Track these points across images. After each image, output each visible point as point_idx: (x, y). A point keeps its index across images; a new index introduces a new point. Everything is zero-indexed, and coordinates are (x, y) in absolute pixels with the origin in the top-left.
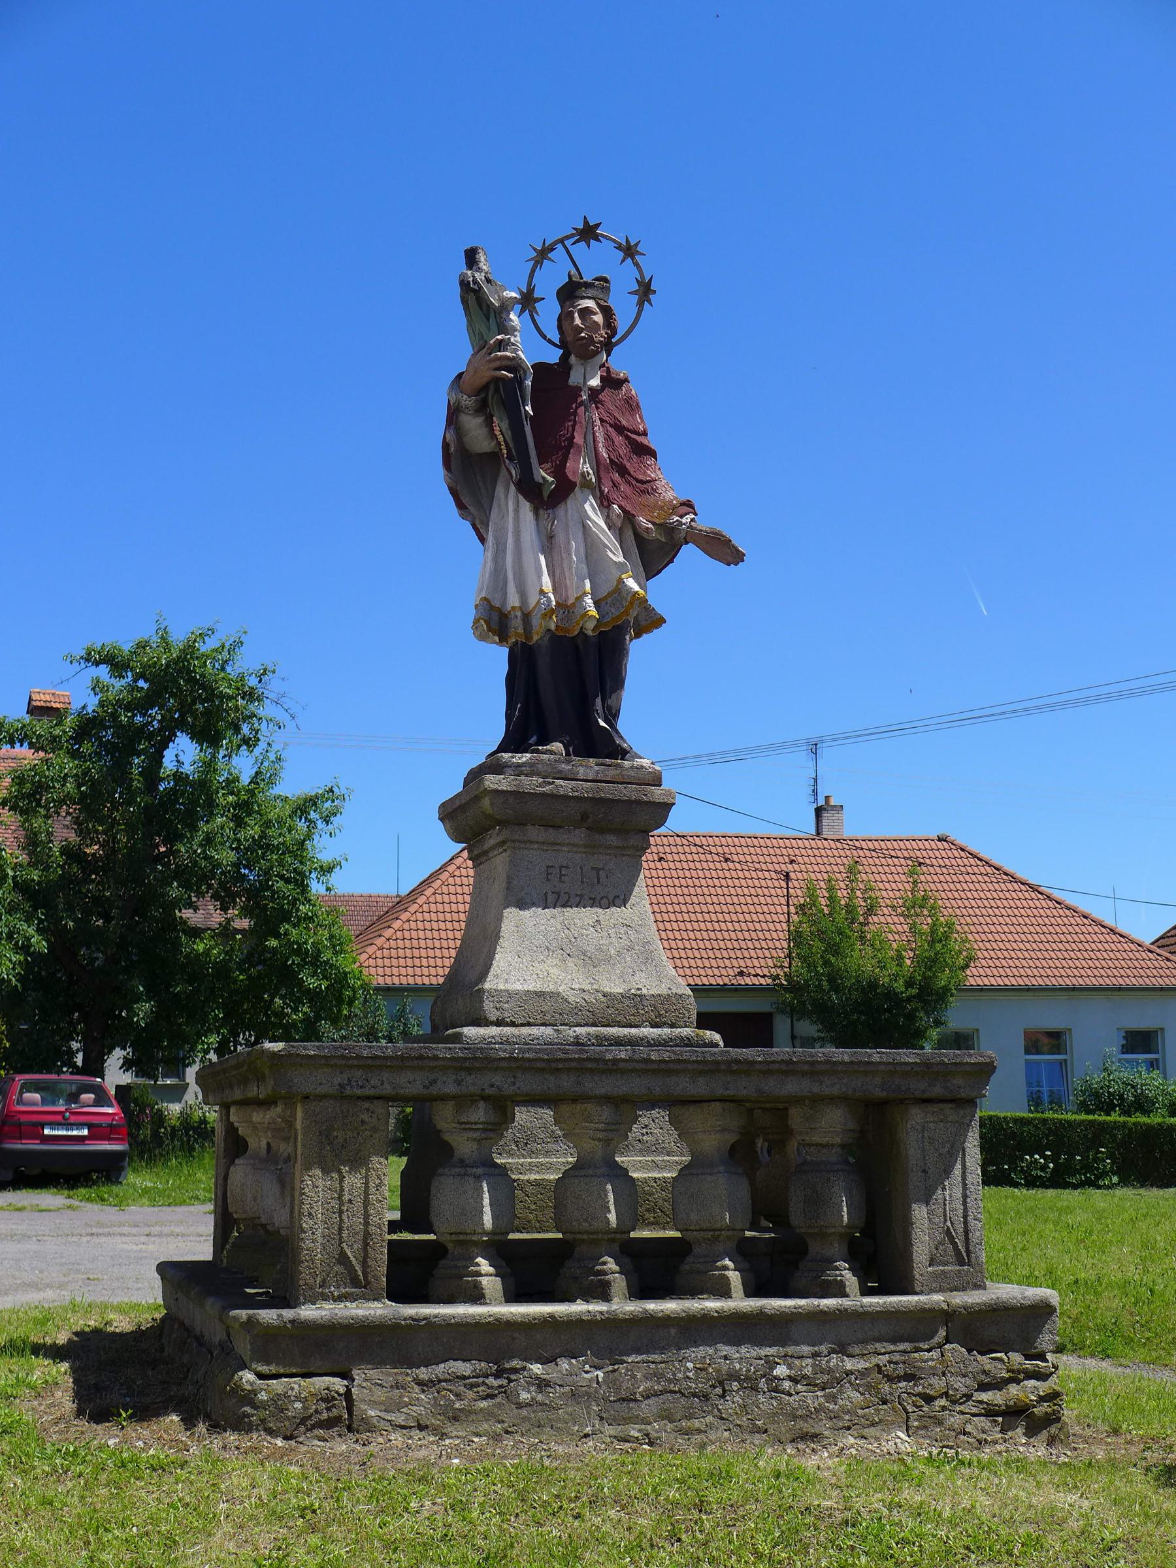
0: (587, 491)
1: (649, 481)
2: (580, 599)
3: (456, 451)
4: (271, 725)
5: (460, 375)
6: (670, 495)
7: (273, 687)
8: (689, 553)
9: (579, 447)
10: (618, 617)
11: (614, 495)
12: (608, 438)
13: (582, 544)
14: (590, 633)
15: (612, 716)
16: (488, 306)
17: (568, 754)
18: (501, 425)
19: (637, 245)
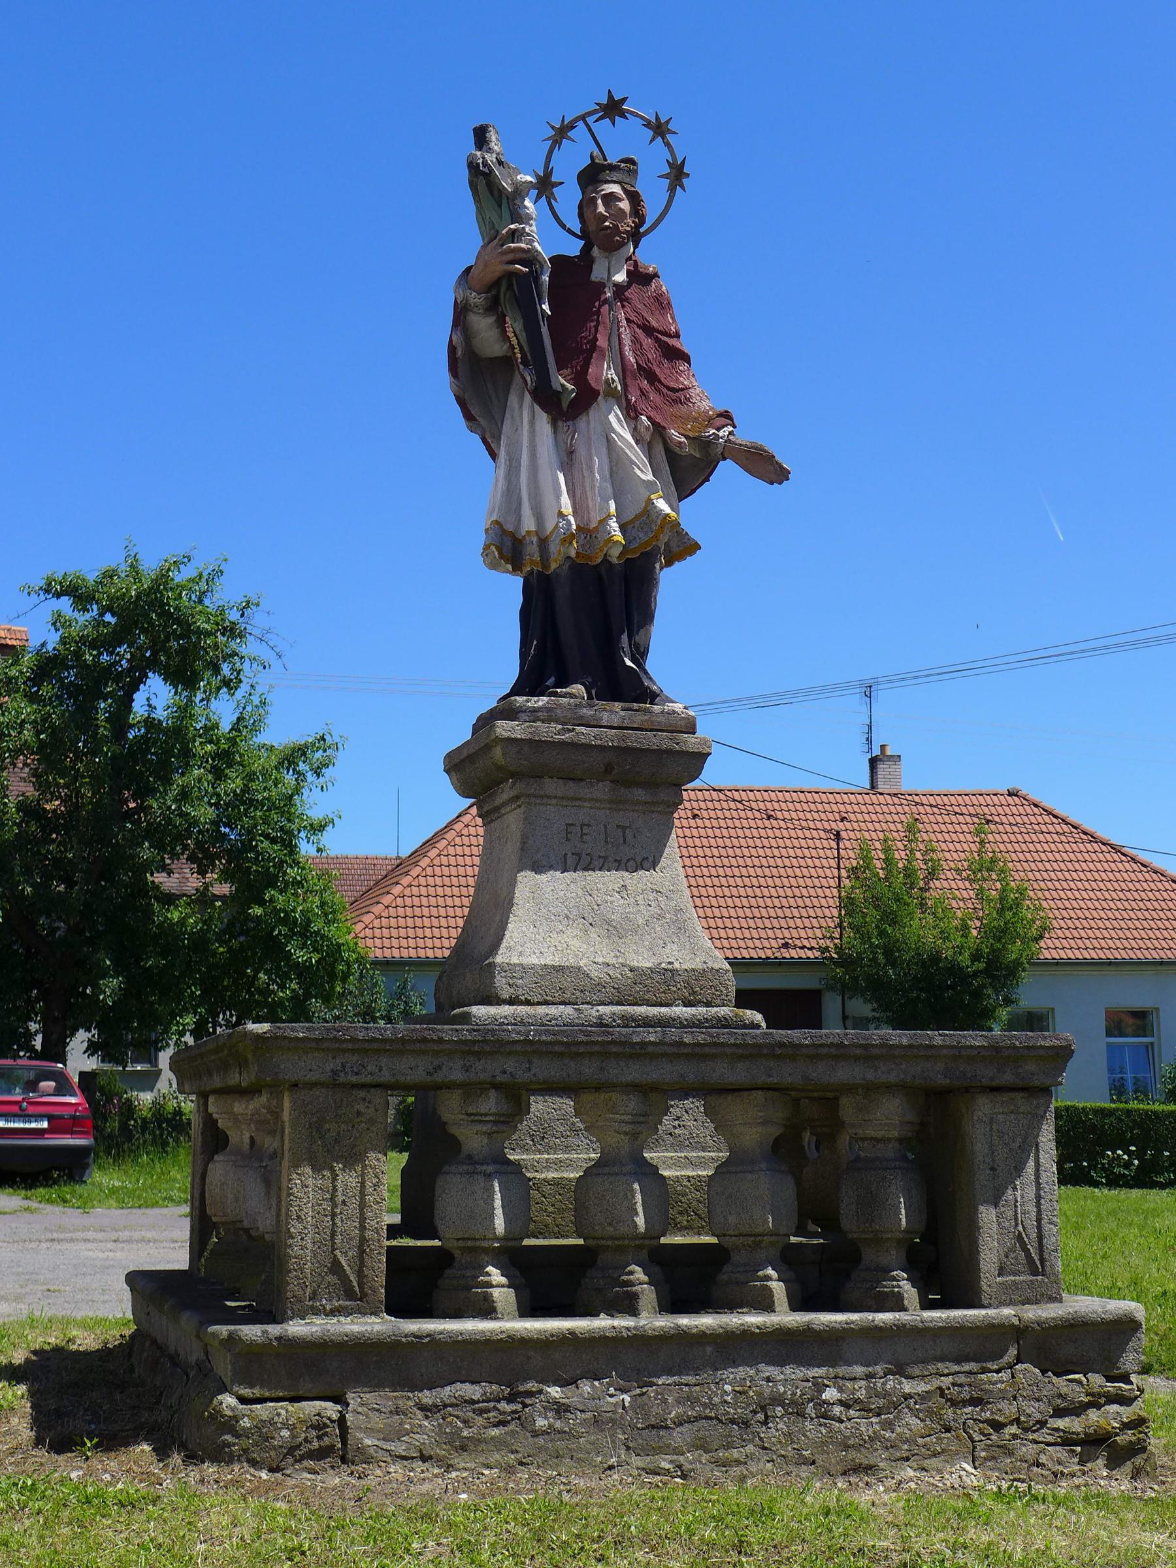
1: (682, 390)
2: (604, 522)
6: (705, 405)
7: (257, 621)
8: (727, 471)
9: (602, 350)
10: (647, 543)
11: (642, 406)
12: (635, 340)
13: (606, 461)
14: (615, 561)
15: (640, 654)
16: (500, 191)
17: (590, 697)
19: (668, 122)
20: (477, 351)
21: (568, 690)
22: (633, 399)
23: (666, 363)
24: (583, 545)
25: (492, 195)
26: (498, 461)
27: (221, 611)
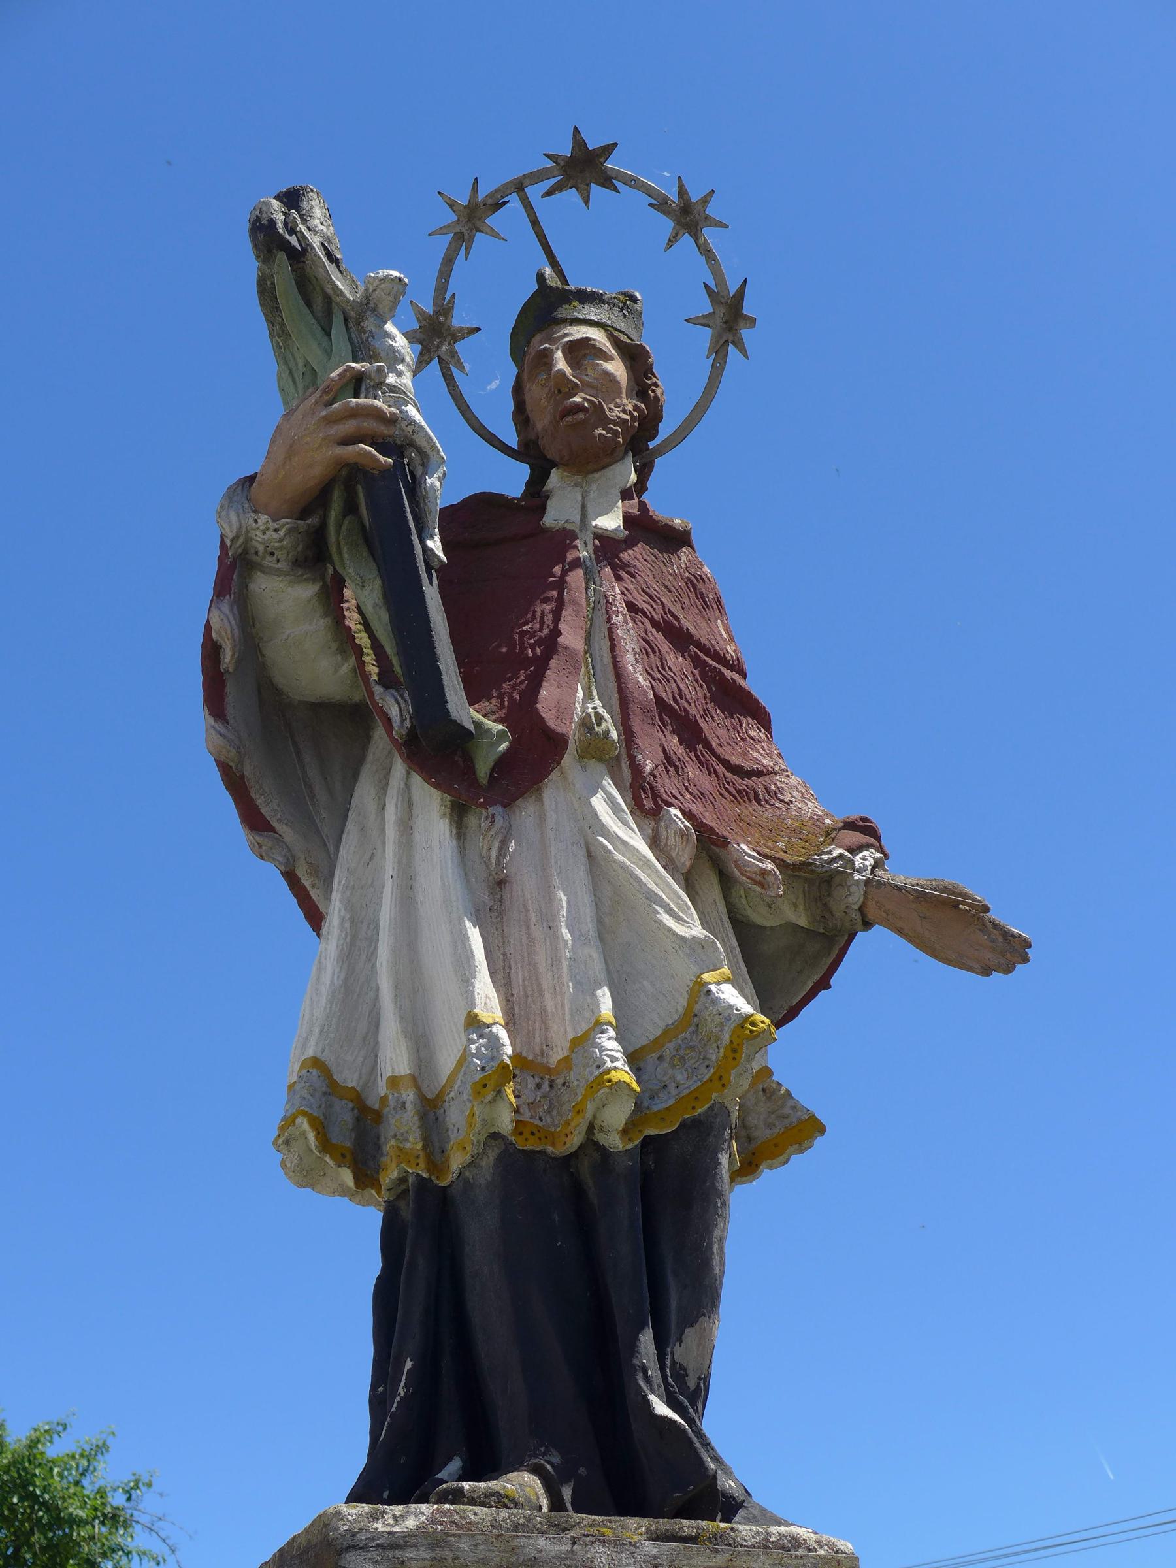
0: (596, 767)
1: (759, 774)
2: (583, 1042)
3: (238, 662)
4: (145, 1561)
5: (251, 479)
6: (812, 807)
7: (148, 1505)
8: (875, 953)
9: (571, 654)
10: (696, 1097)
11: (667, 784)
12: (648, 648)
13: (585, 898)
14: (614, 1142)
15: (690, 1393)
16: (328, 301)
17: (557, 1505)
18: (363, 596)
19: (705, 201)
20: (279, 680)
21: (493, 1485)
22: (649, 766)
23: (719, 715)
24: (531, 1105)
25: (309, 304)
26: (324, 931)
27: (102, 1493)
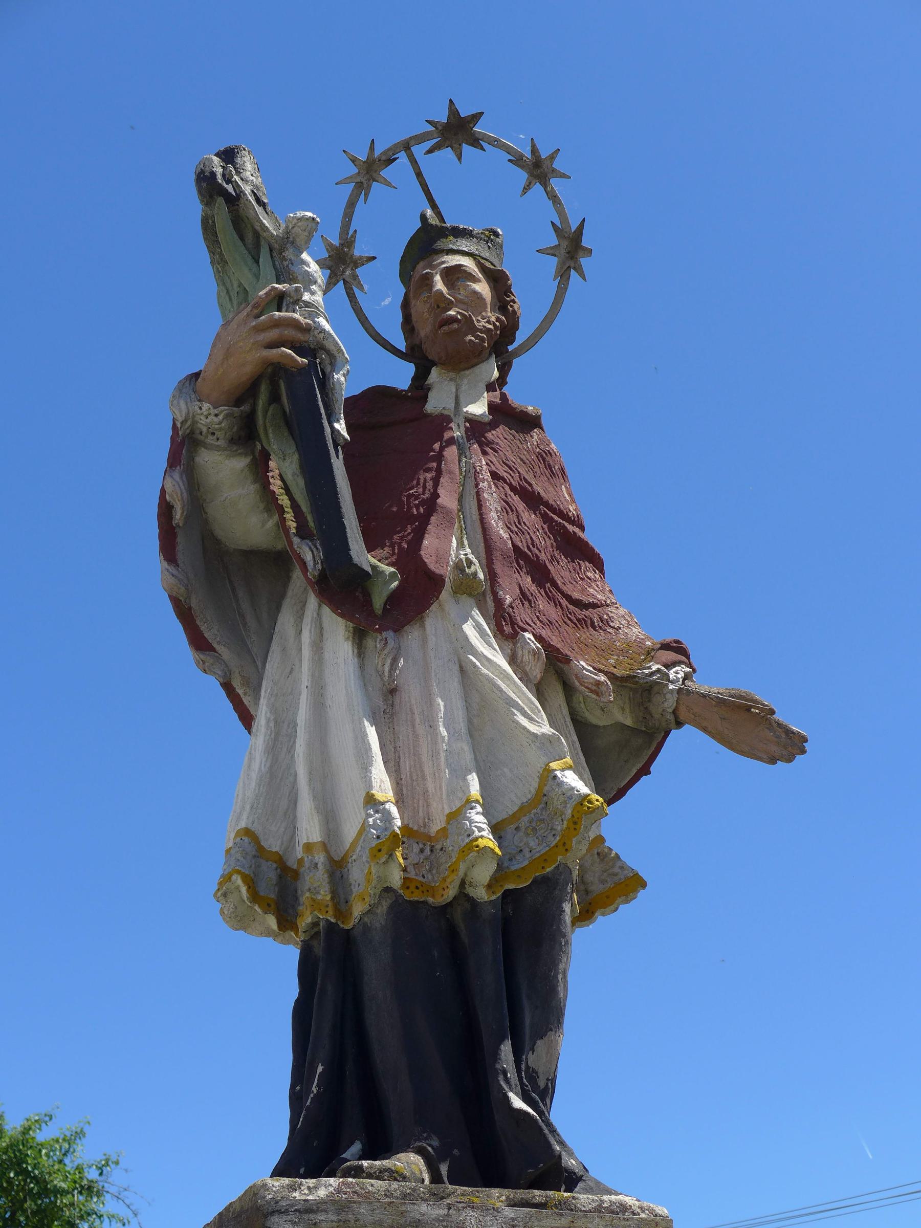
0: (467, 601)
1: (594, 606)
2: (457, 816)
3: (187, 519)
4: (114, 1222)
5: (197, 375)
6: (636, 632)
7: (116, 1178)
8: (686, 746)
9: (447, 512)
10: (545, 859)
11: (522, 614)
12: (508, 507)
13: (458, 703)
14: (481, 894)
15: (540, 1091)
16: (257, 235)
17: (436, 1178)
18: (284, 467)
19: (552, 157)
20: (219, 533)
21: (386, 1163)
22: (508, 600)
23: (563, 560)
24: (416, 865)
25: (242, 238)
26: (254, 729)
27: (80, 1169)
